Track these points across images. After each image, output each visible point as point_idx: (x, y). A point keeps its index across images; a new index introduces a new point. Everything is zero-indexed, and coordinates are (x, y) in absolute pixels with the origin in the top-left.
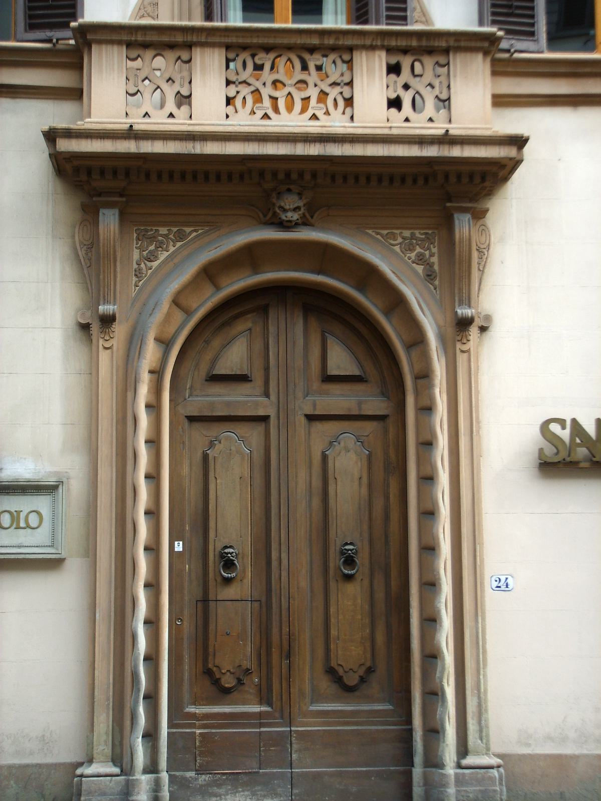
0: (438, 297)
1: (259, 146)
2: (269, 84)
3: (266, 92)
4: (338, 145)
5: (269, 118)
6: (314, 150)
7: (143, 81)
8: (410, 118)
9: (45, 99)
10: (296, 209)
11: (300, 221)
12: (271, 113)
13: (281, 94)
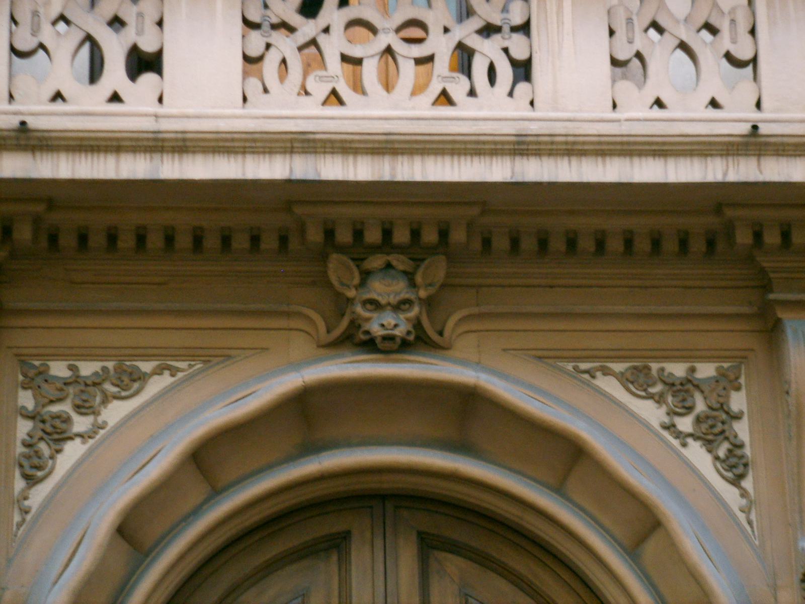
0: (757, 543)
5: (341, 102)
7: (54, 23)
11: (411, 338)
12: (345, 91)
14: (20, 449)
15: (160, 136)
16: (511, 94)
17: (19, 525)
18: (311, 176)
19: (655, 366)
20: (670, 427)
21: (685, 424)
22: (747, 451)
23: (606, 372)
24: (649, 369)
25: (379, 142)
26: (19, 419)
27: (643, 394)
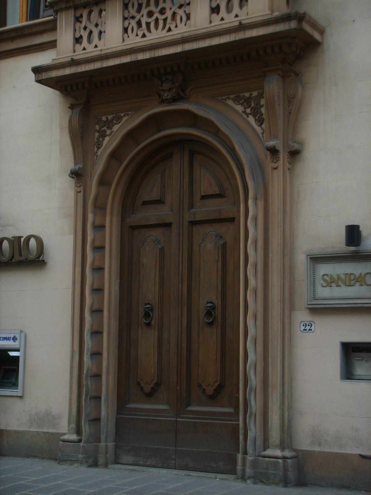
1: (70, 69)
2: (145, 15)
3: (144, 21)
4: (196, 42)
6: (126, 60)
8: (238, 14)
9: (27, 54)
10: (170, 90)
13: (152, 20)
14: (96, 140)
15: (102, 56)
16: (185, 25)
17: (96, 160)
18: (136, 60)
19: (241, 95)
20: (244, 112)
21: (248, 111)
22: (264, 116)
23: (229, 98)
24: (240, 96)
25: (149, 47)
26: (96, 133)
27: (238, 103)
